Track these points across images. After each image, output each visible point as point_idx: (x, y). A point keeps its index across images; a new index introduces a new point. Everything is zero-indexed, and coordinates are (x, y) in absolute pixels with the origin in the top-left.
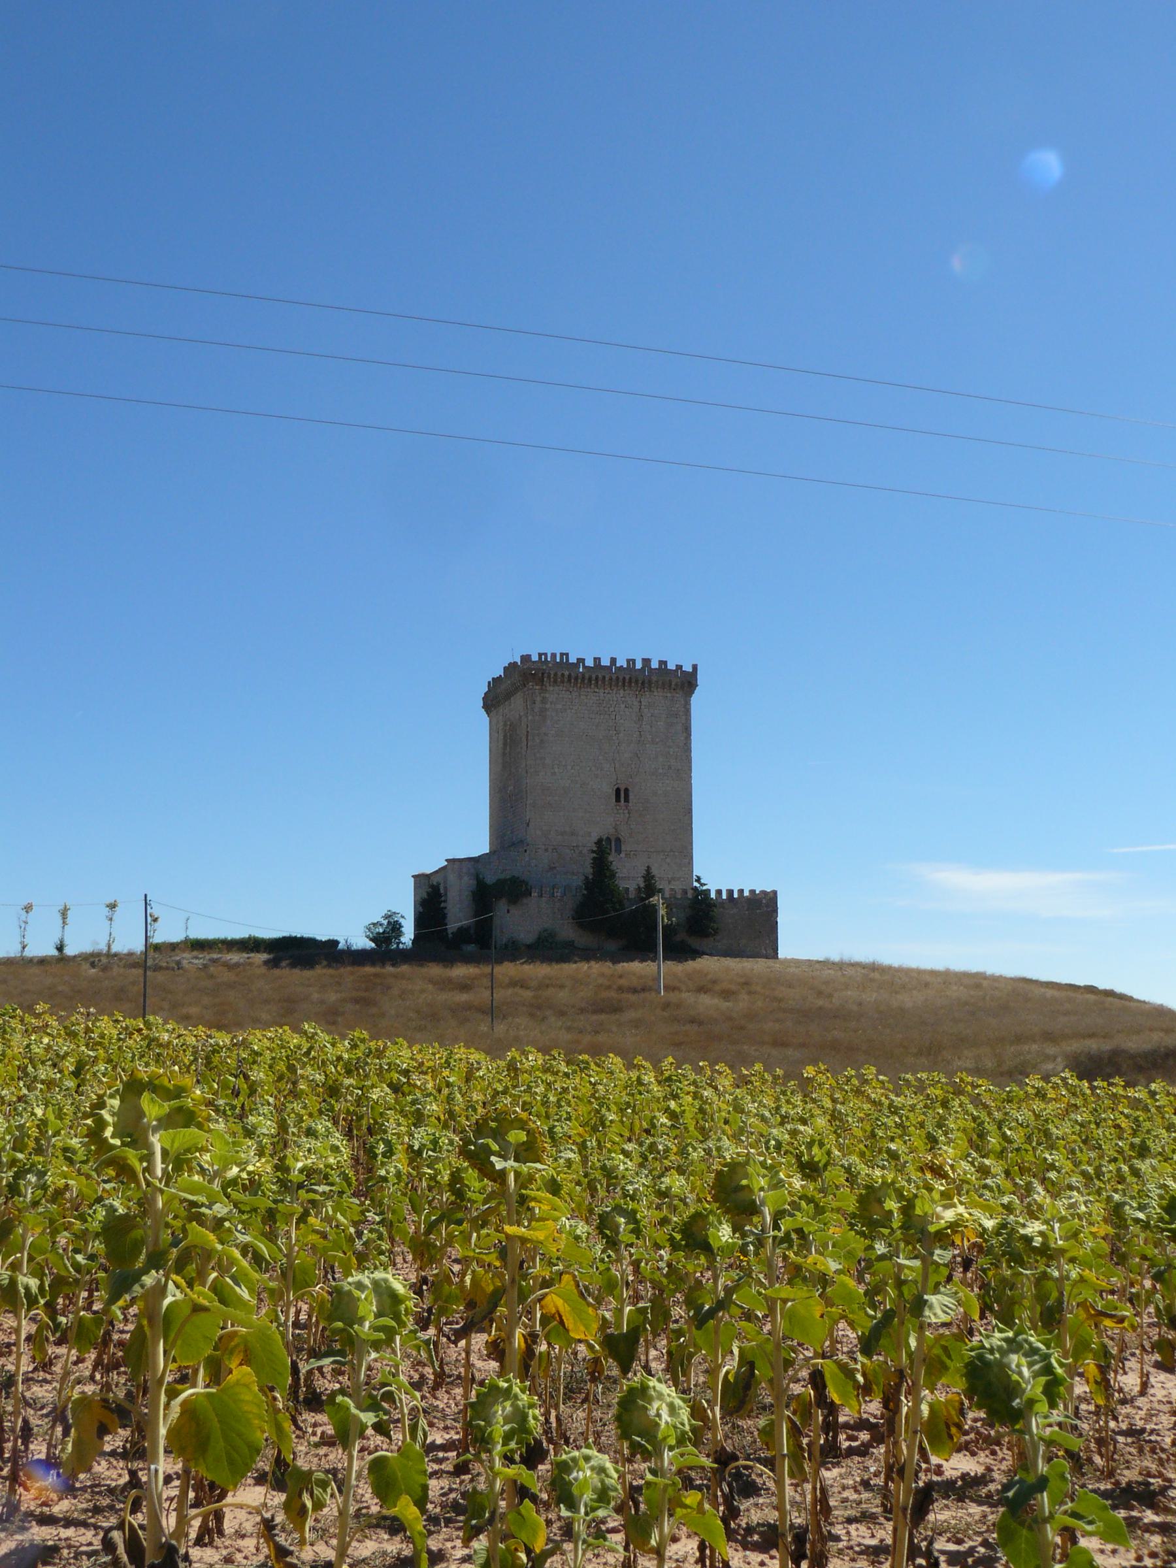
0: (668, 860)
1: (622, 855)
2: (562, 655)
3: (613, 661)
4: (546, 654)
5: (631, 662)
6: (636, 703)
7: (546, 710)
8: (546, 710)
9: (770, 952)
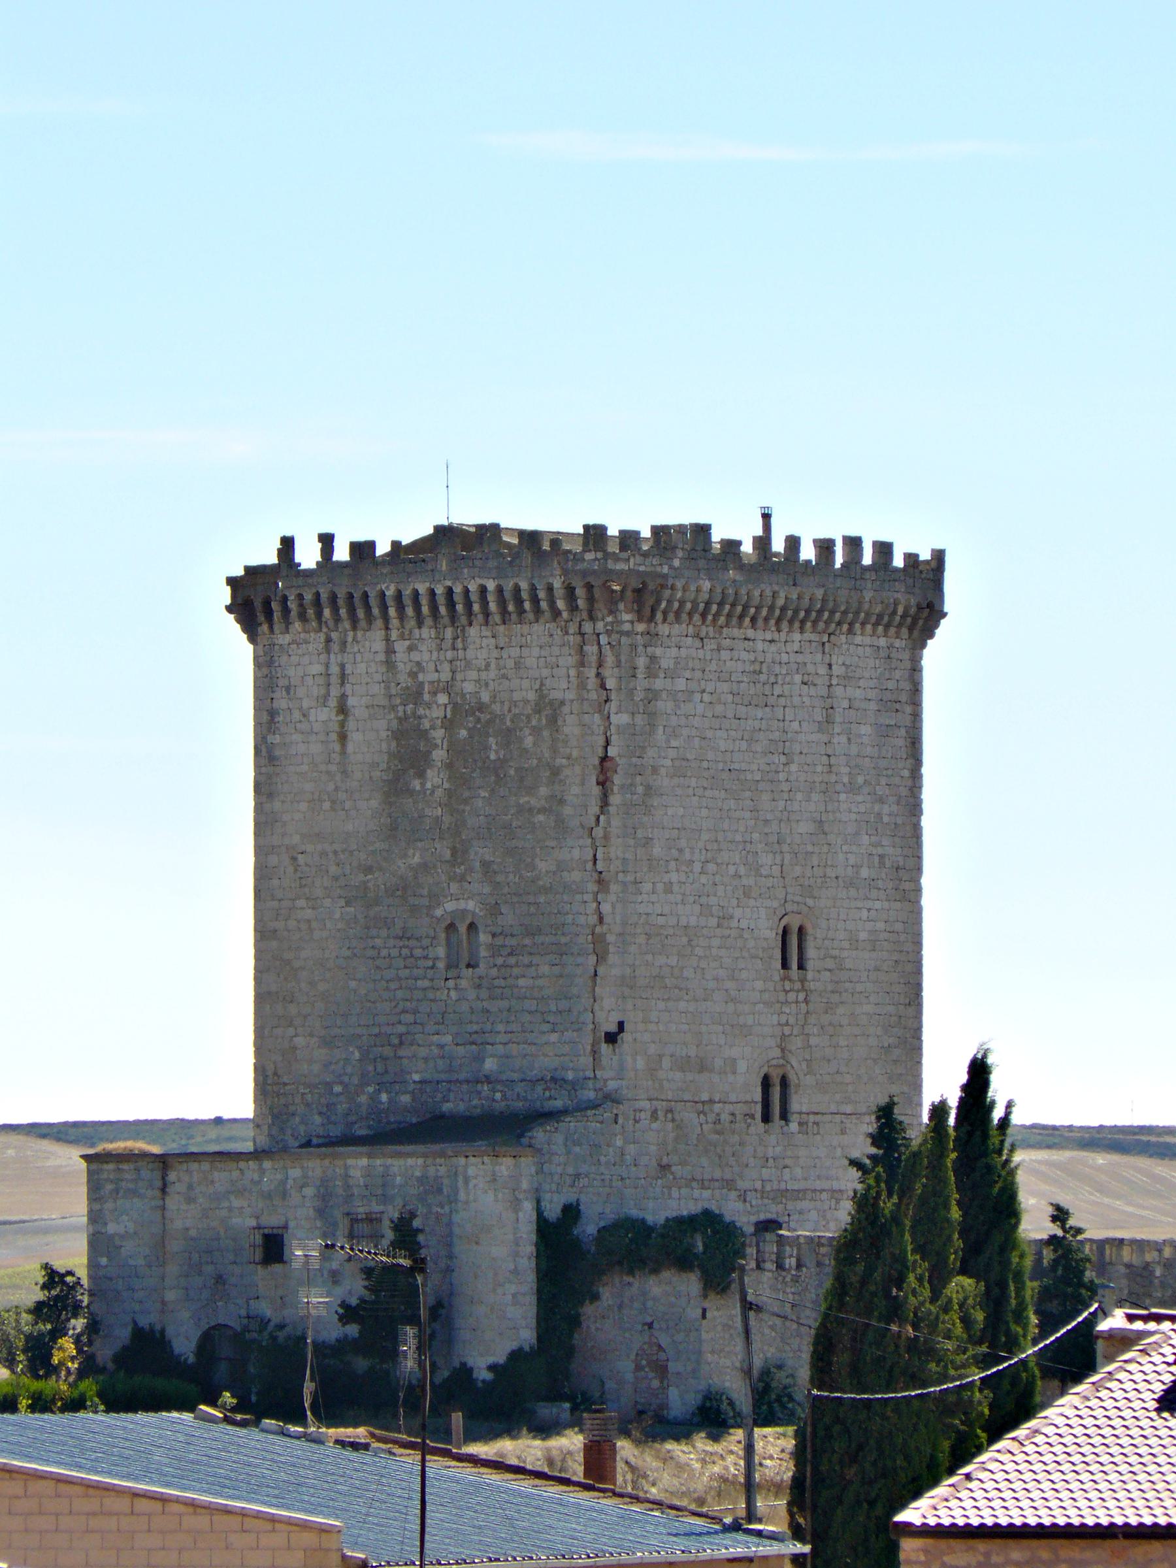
1: (794, 1126)
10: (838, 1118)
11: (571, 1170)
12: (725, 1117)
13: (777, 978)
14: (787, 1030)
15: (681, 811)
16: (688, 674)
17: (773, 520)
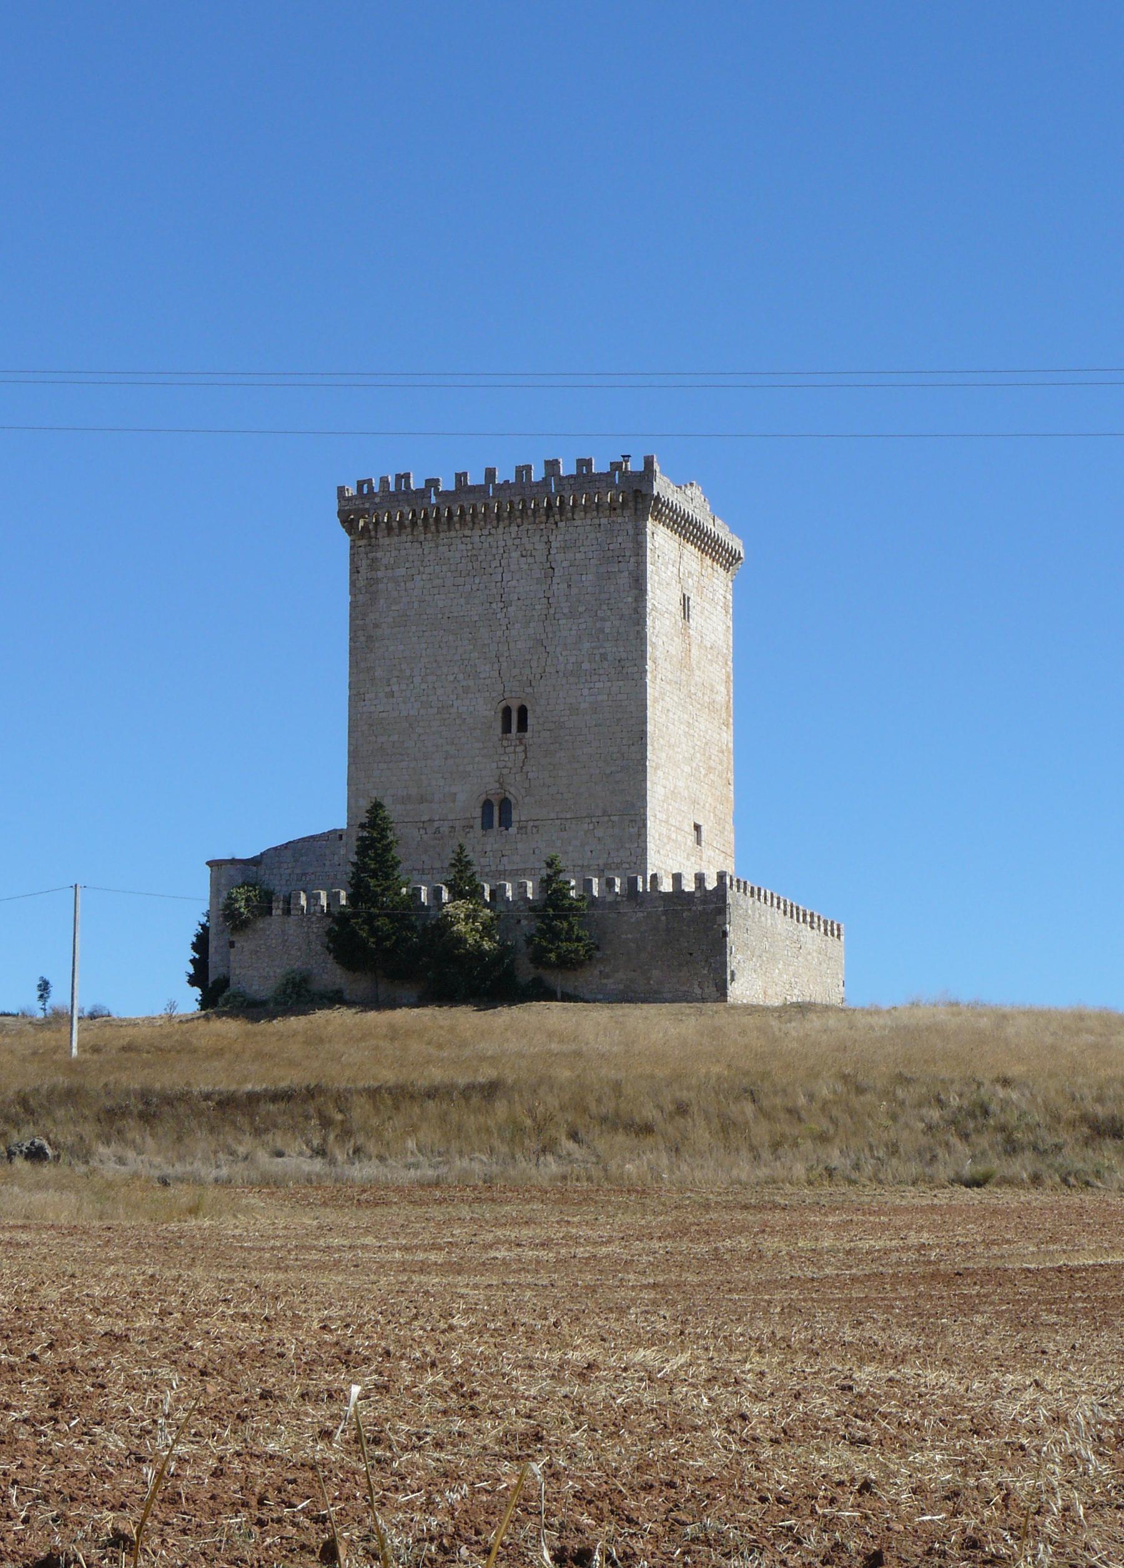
0: (599, 832)
1: (513, 830)
2: (399, 477)
3: (490, 474)
4: (369, 481)
5: (523, 471)
6: (541, 546)
7: (377, 581)
8: (377, 581)
9: (711, 990)
10: (558, 822)
11: (298, 871)
12: (445, 829)
13: (496, 739)
14: (505, 771)
15: (402, 647)
16: (407, 565)
17: (438, 459)
